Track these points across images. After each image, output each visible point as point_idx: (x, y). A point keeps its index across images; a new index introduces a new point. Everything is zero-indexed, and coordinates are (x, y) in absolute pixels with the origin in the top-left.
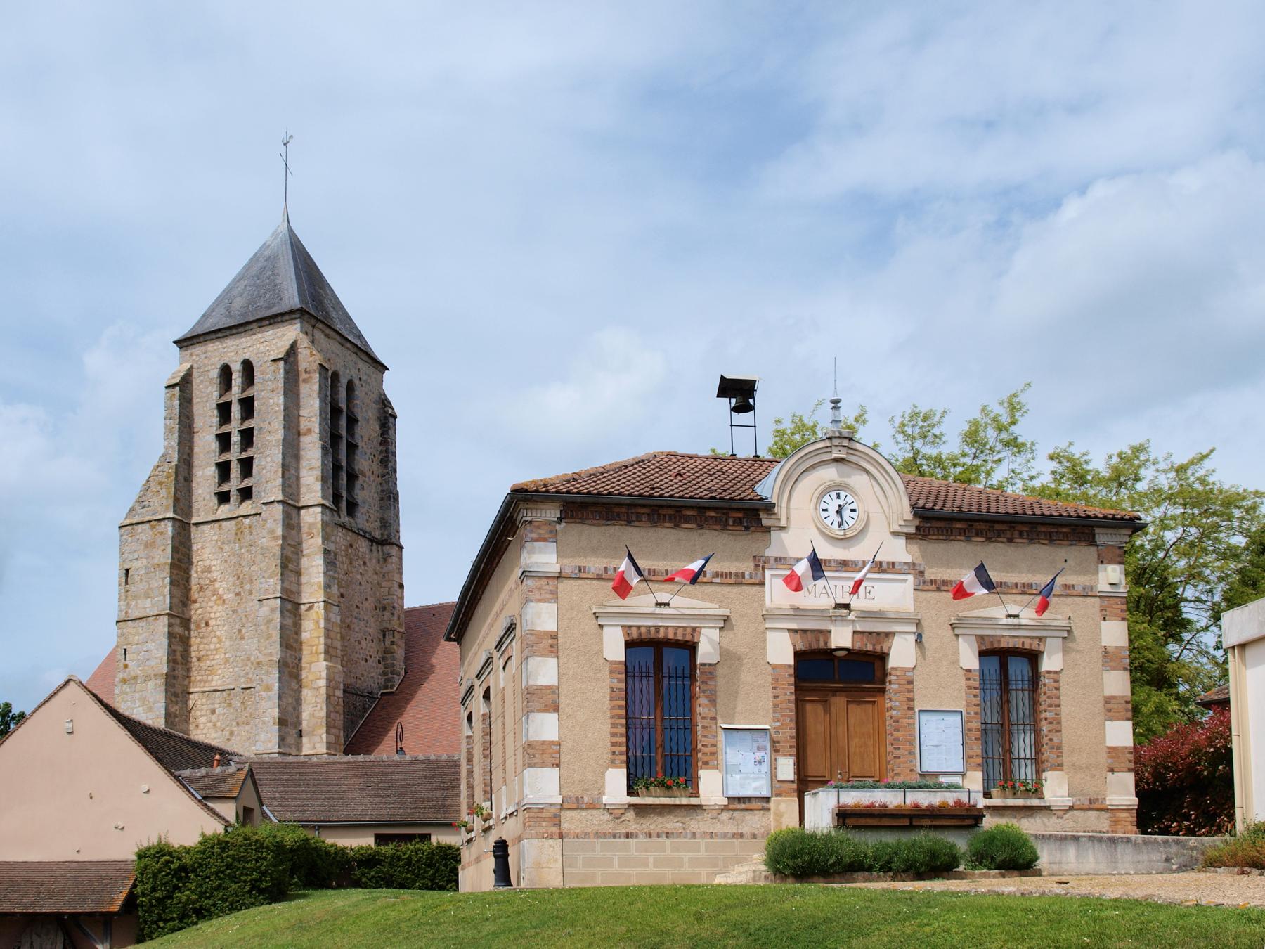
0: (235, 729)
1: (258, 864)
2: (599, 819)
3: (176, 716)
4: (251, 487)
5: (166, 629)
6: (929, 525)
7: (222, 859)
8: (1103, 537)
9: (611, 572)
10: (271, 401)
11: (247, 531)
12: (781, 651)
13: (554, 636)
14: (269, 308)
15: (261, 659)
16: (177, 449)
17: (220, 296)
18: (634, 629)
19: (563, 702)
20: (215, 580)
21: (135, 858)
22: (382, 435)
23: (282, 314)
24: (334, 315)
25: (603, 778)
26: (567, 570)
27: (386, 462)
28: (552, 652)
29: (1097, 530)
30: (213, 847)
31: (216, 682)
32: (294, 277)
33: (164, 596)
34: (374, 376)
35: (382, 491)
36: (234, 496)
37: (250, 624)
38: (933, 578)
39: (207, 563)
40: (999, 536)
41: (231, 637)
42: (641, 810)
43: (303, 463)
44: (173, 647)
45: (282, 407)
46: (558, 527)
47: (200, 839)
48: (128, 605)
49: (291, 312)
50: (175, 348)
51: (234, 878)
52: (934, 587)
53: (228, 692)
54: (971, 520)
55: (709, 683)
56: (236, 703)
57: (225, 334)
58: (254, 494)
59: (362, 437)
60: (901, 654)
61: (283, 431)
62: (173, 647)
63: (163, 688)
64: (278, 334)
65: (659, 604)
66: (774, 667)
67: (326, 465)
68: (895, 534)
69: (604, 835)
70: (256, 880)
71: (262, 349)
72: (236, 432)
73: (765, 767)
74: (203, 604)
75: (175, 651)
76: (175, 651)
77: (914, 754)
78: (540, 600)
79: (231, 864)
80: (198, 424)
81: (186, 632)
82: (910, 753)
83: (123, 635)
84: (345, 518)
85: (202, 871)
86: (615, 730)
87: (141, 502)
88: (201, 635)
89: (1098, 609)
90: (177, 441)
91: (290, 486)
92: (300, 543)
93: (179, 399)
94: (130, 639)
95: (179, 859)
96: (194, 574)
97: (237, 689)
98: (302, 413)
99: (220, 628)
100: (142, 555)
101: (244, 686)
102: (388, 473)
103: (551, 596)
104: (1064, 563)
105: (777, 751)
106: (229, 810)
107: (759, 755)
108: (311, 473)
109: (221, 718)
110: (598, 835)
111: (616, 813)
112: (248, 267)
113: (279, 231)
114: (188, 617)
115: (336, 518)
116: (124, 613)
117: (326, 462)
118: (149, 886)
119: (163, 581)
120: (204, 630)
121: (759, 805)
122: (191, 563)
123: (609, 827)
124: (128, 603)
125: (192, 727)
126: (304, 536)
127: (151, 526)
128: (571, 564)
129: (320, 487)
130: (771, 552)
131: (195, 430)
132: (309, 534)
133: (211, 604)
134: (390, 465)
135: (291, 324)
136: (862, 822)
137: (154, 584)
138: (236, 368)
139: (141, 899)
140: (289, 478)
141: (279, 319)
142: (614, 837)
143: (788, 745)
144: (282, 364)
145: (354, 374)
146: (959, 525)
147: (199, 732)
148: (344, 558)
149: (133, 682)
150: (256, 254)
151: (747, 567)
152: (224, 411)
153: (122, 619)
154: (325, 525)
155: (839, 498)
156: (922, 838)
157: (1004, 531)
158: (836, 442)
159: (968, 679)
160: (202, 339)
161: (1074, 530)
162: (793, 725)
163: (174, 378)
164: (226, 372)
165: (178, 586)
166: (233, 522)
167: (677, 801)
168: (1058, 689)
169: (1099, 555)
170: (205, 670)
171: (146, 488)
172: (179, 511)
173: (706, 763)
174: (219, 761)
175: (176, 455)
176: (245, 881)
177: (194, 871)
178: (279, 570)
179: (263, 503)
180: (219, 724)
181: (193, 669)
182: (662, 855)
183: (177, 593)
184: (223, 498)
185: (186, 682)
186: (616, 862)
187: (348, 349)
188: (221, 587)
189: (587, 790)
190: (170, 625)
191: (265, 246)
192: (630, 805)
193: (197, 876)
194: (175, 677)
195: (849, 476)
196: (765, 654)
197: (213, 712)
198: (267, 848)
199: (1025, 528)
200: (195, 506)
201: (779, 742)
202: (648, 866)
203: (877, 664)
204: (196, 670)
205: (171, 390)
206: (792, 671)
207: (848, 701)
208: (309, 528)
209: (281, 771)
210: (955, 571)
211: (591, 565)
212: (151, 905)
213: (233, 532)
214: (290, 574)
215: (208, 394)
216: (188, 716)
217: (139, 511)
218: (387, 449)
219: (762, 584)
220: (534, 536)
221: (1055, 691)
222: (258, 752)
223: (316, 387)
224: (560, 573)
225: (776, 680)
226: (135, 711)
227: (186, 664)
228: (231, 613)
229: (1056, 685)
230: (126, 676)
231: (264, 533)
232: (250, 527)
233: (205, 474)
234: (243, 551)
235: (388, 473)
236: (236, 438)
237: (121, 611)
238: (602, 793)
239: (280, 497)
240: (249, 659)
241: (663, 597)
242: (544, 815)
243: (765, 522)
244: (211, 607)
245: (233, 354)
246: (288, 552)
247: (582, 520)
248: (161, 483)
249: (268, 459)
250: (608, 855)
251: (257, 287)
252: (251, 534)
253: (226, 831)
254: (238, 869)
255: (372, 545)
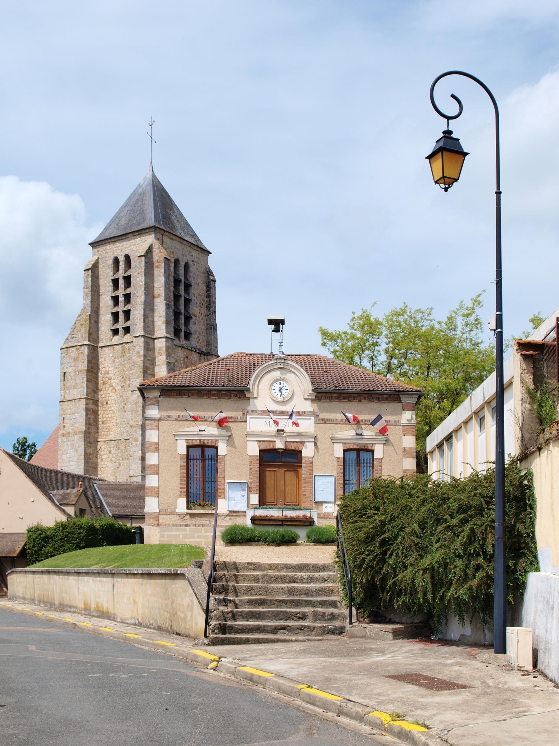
0: (121, 462)
1: (79, 536)
2: (174, 519)
3: (90, 454)
4: (129, 327)
5: (85, 407)
6: (321, 395)
7: (63, 533)
8: (404, 399)
9: (181, 417)
10: (138, 279)
11: (127, 351)
12: (254, 450)
13: (157, 444)
14: (139, 225)
15: (133, 424)
16: (90, 305)
17: (115, 216)
18: (190, 441)
19: (161, 470)
20: (111, 379)
21: (26, 532)
22: (207, 292)
23: (145, 229)
24: (177, 225)
25: (176, 502)
26: (163, 417)
27: (210, 307)
28: (156, 450)
29: (401, 396)
30: (59, 528)
31: (112, 436)
32: (153, 206)
33: (84, 388)
34: (202, 258)
35: (207, 324)
36: (121, 331)
37: (129, 404)
38: (323, 418)
39: (107, 369)
40: (354, 399)
41: (119, 411)
42: (192, 515)
43: (156, 314)
44: (89, 416)
45: (144, 283)
46: (159, 399)
47: (55, 524)
48: (65, 393)
49: (149, 228)
50: (90, 247)
51: (68, 542)
52: (323, 422)
53: (118, 441)
54: (340, 393)
55: (222, 463)
56: (122, 448)
57: (115, 240)
58: (131, 330)
59: (194, 294)
60: (308, 451)
61: (144, 296)
62: (89, 416)
63: (83, 439)
64: (143, 240)
65: (200, 431)
66: (250, 456)
67: (168, 314)
68: (305, 399)
69: (176, 525)
70: (78, 543)
71: (135, 249)
72: (122, 295)
73: (246, 498)
74: (105, 392)
75: (90, 418)
76: (90, 418)
77: (312, 493)
78: (152, 429)
79: (67, 535)
80: (102, 290)
81: (96, 408)
82: (310, 493)
83: (62, 409)
84: (183, 342)
85: (55, 538)
86: (182, 482)
87: (72, 335)
88: (104, 409)
89: (401, 431)
90: (90, 300)
91: (148, 327)
92: (154, 359)
93: (91, 277)
94: (66, 412)
95: (45, 533)
96: (100, 375)
97: (123, 440)
98: (156, 285)
99: (114, 405)
100: (73, 364)
101: (126, 438)
102: (210, 314)
103: (156, 427)
104: (385, 411)
105: (251, 492)
106: (71, 510)
107: (243, 493)
108: (160, 319)
109: (114, 455)
110: (174, 525)
111: (182, 516)
112: (130, 199)
113: (147, 177)
114: (97, 399)
115: (177, 342)
116: (63, 397)
117: (169, 313)
118: (31, 545)
119: (83, 379)
120: (105, 406)
121: (242, 514)
122: (98, 369)
123: (178, 522)
124: (65, 392)
125: (99, 460)
126: (157, 355)
127: (77, 349)
128: (164, 414)
129: (165, 327)
130: (250, 408)
131: (101, 294)
132: (159, 353)
133: (109, 392)
134: (211, 309)
135: (150, 235)
136: (261, 522)
137: (79, 381)
138: (122, 259)
139: (28, 551)
140: (148, 322)
141: (143, 232)
142: (181, 526)
143: (256, 489)
144: (143, 258)
145: (189, 258)
146: (335, 395)
147: (103, 463)
148: (183, 365)
149: (68, 435)
150: (134, 191)
151: (239, 414)
152: (115, 282)
153: (62, 400)
154: (167, 348)
155: (280, 384)
156: (282, 530)
157: (356, 397)
158: (279, 361)
159: (338, 462)
160: (103, 242)
161: (390, 396)
162: (258, 481)
163: (88, 265)
164: (116, 261)
165: (91, 382)
166: (120, 346)
167: (207, 512)
168: (381, 466)
169: (403, 407)
170: (106, 429)
171: (74, 328)
172: (91, 340)
173: (220, 496)
174: (81, 485)
175: (90, 308)
176: (74, 543)
177: (51, 538)
178: (142, 374)
179: (134, 337)
180: (113, 459)
181: (100, 428)
182: (200, 534)
183: (91, 386)
184: (115, 332)
185: (96, 436)
186: (181, 537)
187: (185, 245)
188: (114, 382)
189: (170, 507)
190: (87, 404)
191: (139, 186)
192: (187, 513)
193: (53, 540)
194: (90, 433)
195: (286, 375)
196: (247, 451)
197: (110, 452)
198: (84, 528)
199: (366, 396)
200: (101, 336)
201: (251, 488)
202: (194, 538)
203: (299, 454)
204: (102, 429)
205: (87, 272)
206: (258, 458)
207: (285, 471)
208: (159, 350)
209: (118, 489)
210: (334, 414)
211: (173, 414)
212: (33, 554)
213: (120, 352)
214: (149, 376)
215: (107, 274)
216: (97, 454)
217: (71, 340)
218: (210, 300)
219: (246, 421)
220: (150, 403)
221: (379, 467)
222: (131, 475)
223: (163, 271)
224: (160, 418)
225: (251, 462)
226: (69, 451)
227: (96, 425)
228: (119, 397)
229: (380, 464)
230: (64, 432)
231: (134, 354)
232: (129, 349)
233: (106, 319)
234: (125, 362)
235: (210, 314)
236: (121, 299)
237: (61, 396)
238: (176, 508)
239: (142, 334)
240: (128, 423)
241: (202, 428)
242: (152, 516)
243: (247, 395)
244: (109, 394)
245: (120, 251)
246: (147, 364)
247: (169, 396)
248: (82, 325)
249: (138, 312)
250: (178, 533)
251: (133, 212)
252: (129, 353)
253: (68, 520)
254: (70, 538)
255: (201, 356)
